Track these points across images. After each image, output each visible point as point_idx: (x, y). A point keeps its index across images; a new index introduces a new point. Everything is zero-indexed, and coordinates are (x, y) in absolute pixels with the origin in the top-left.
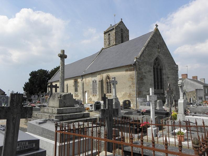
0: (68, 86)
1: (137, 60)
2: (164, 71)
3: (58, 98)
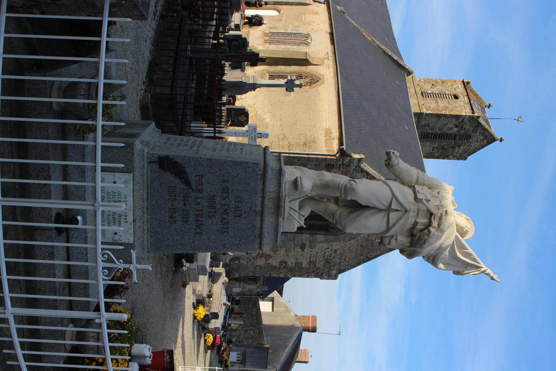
1: (356, 160)
2: (323, 236)
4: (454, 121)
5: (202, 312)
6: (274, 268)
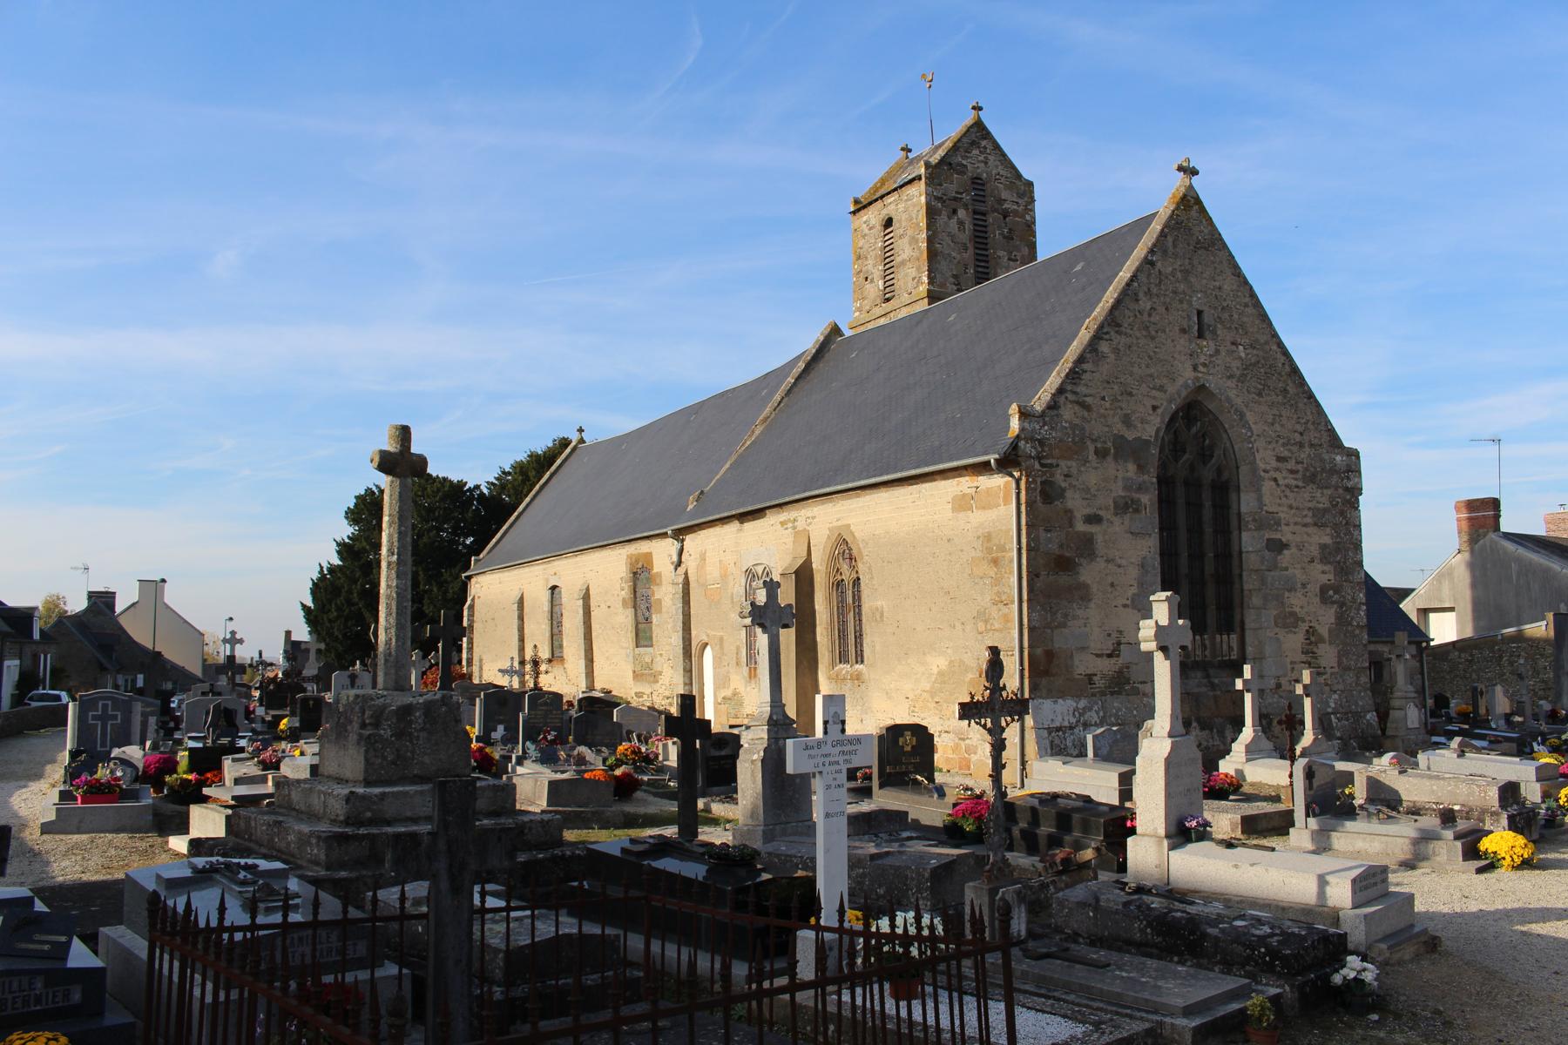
0: (593, 603)
1: (1026, 425)
3: (363, 726)
4: (943, 218)
5: (1502, 841)
6: (1342, 620)
